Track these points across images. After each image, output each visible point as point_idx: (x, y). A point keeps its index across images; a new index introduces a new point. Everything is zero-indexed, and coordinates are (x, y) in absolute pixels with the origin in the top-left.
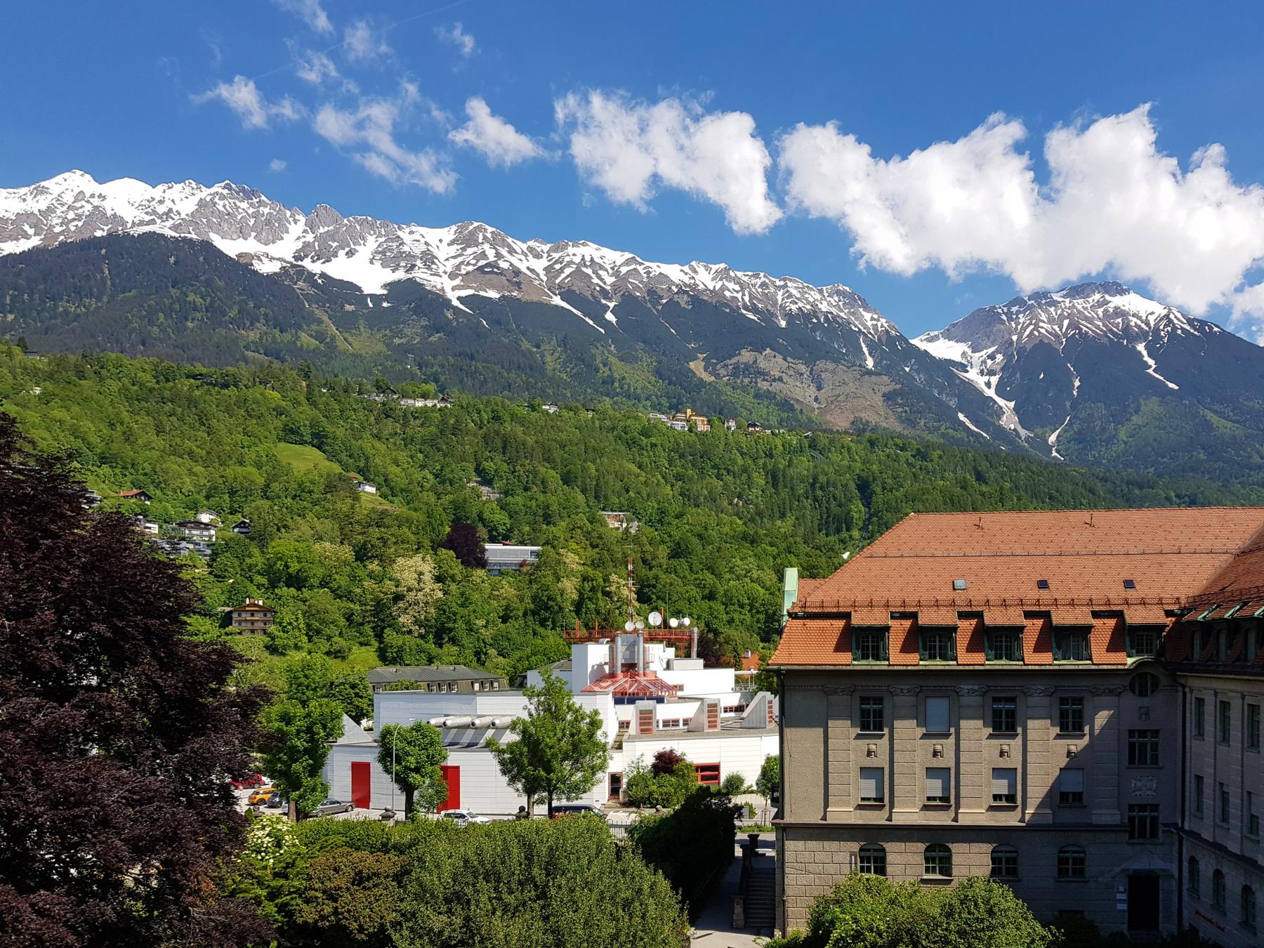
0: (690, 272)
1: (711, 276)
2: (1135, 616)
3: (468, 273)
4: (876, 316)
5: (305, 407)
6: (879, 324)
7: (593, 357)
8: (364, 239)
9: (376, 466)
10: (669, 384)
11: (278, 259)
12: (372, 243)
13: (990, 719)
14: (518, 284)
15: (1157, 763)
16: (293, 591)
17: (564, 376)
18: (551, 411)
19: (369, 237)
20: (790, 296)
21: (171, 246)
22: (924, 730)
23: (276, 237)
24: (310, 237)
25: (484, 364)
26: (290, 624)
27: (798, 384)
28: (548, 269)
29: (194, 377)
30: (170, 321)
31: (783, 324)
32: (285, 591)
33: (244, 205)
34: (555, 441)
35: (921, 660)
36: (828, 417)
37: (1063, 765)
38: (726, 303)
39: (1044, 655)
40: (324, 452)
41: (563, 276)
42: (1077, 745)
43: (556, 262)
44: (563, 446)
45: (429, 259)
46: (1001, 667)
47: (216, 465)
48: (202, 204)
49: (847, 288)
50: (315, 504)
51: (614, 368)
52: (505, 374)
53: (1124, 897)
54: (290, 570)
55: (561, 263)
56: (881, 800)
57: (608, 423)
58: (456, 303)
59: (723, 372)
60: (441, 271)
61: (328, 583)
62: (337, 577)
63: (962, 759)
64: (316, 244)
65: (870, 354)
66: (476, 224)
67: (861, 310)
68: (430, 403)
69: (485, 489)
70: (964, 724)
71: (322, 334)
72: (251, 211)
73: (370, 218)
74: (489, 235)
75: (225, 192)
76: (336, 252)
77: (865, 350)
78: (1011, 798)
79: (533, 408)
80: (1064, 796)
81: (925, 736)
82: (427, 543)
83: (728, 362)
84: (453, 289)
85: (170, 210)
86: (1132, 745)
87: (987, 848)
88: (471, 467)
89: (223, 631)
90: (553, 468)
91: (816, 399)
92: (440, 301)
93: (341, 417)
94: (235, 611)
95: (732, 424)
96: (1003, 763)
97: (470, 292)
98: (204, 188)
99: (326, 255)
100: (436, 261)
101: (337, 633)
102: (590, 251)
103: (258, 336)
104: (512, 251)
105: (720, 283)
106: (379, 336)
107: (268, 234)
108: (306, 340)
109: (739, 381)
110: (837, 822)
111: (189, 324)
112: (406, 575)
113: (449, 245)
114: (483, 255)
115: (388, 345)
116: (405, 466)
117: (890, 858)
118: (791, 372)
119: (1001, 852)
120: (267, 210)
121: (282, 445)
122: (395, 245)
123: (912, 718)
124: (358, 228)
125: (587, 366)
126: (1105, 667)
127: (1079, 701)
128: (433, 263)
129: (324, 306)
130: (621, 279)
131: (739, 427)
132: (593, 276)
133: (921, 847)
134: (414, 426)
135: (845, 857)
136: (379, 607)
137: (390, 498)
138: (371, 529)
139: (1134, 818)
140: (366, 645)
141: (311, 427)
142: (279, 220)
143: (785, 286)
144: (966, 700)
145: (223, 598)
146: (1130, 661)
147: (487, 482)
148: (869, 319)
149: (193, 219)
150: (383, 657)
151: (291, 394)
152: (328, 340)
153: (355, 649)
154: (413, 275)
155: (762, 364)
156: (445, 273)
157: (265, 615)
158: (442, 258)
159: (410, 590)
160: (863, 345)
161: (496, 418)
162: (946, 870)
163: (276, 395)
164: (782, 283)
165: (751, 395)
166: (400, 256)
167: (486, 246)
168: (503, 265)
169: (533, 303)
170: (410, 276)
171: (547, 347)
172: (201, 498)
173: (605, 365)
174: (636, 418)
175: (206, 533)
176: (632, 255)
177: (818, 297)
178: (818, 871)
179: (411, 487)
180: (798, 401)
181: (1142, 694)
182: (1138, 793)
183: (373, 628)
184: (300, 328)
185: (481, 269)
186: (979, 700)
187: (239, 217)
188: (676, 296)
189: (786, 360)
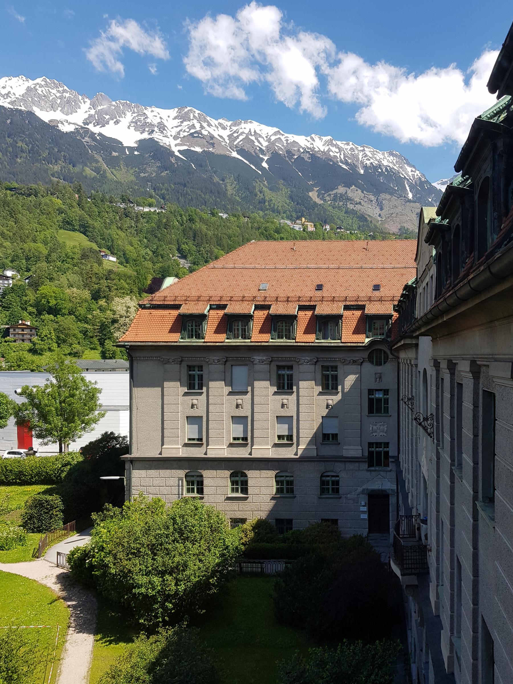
0: (311, 140)
1: (323, 143)
2: (372, 309)
3: (184, 137)
4: (414, 170)
5: (77, 209)
6: (416, 175)
7: (254, 187)
8: (125, 114)
9: (118, 245)
10: (297, 204)
11: (73, 124)
12: (129, 117)
13: (275, 380)
14: (213, 145)
15: (388, 412)
16: (52, 317)
17: (237, 198)
18: (224, 217)
19: (127, 113)
20: (366, 156)
21: (8, 113)
22: (230, 389)
23: (73, 111)
24: (93, 112)
25: (191, 190)
26: (46, 336)
27: (370, 206)
28: (230, 136)
29: (11, 189)
30: (5, 157)
31: (362, 172)
32: (47, 317)
33: (54, 91)
34: (225, 234)
35: (227, 339)
36: (386, 226)
37: (324, 414)
38: (330, 159)
39: (309, 336)
40: (87, 236)
41: (238, 140)
42: (334, 399)
43: (235, 132)
44: (230, 237)
45: (162, 127)
46: (279, 344)
47: (19, 242)
48: (29, 89)
49: (398, 153)
50: (74, 265)
51: (266, 194)
52: (203, 196)
53: (365, 509)
54: (50, 305)
55: (237, 133)
56: (200, 439)
57: (256, 225)
58: (177, 154)
59: (328, 198)
60: (169, 135)
61: (74, 313)
62: (79, 308)
63: (256, 410)
64: (96, 115)
65: (410, 191)
66: (189, 108)
67: (406, 165)
68: (152, 210)
69: (182, 261)
70: (257, 384)
71: (98, 169)
72: (58, 95)
73: (128, 102)
74: (197, 115)
75: (43, 83)
76: (108, 122)
77: (408, 188)
78: (290, 437)
79: (213, 214)
80: (326, 437)
81: (230, 393)
82: (136, 289)
83: (331, 193)
84: (176, 145)
85: (9, 92)
86: (371, 401)
87: (272, 473)
88: (174, 247)
89: (3, 340)
90: (223, 250)
91: (380, 215)
92: (167, 152)
93: (99, 216)
94: (11, 328)
95: (328, 227)
96: (284, 413)
97: (186, 148)
98: (30, 81)
99: (103, 123)
100: (166, 128)
101: (76, 342)
102: (254, 126)
103: (60, 168)
104: (209, 125)
105: (328, 147)
106: (132, 171)
107: (68, 109)
108: (88, 171)
109: (337, 204)
110: (143, 456)
111: (19, 160)
112: (119, 308)
113: (173, 119)
114: (193, 126)
115: (137, 177)
116: (136, 246)
117: (206, 482)
118: (366, 200)
119: (283, 476)
120: (67, 95)
121: (62, 231)
122: (142, 118)
123: (221, 380)
124: (122, 107)
125: (250, 193)
126: (349, 344)
127: (335, 368)
128: (164, 129)
129: (100, 152)
130: (272, 144)
131: (331, 229)
132: (256, 141)
133: (227, 473)
134: (144, 224)
135: (174, 481)
136: (103, 327)
137: (125, 264)
138: (102, 281)
139: (373, 452)
140: (94, 349)
141: (80, 221)
142: (75, 101)
143: (364, 150)
144: (259, 367)
145: (5, 320)
146: (367, 340)
147: (184, 257)
148: (410, 171)
149: (23, 98)
150: (104, 356)
151: (68, 201)
152: (102, 172)
153: (86, 352)
154: (153, 136)
155: (350, 194)
156: (171, 136)
157: (31, 331)
158: (169, 128)
159: (121, 317)
160: (407, 186)
161: (191, 220)
162: (245, 490)
163: (59, 201)
164: (362, 149)
165: (343, 212)
166: (145, 124)
167: (195, 122)
168: (205, 133)
169: (221, 155)
170: (151, 137)
171: (228, 181)
172: (7, 261)
173: (261, 192)
174: (272, 222)
175: (6, 282)
176: (277, 130)
177: (382, 157)
178: (155, 492)
179: (138, 258)
180: (369, 216)
181: (379, 364)
182: (375, 434)
183: (98, 339)
184: (86, 165)
185: (192, 134)
186: (267, 367)
187: (51, 98)
188: (302, 154)
189: (363, 193)
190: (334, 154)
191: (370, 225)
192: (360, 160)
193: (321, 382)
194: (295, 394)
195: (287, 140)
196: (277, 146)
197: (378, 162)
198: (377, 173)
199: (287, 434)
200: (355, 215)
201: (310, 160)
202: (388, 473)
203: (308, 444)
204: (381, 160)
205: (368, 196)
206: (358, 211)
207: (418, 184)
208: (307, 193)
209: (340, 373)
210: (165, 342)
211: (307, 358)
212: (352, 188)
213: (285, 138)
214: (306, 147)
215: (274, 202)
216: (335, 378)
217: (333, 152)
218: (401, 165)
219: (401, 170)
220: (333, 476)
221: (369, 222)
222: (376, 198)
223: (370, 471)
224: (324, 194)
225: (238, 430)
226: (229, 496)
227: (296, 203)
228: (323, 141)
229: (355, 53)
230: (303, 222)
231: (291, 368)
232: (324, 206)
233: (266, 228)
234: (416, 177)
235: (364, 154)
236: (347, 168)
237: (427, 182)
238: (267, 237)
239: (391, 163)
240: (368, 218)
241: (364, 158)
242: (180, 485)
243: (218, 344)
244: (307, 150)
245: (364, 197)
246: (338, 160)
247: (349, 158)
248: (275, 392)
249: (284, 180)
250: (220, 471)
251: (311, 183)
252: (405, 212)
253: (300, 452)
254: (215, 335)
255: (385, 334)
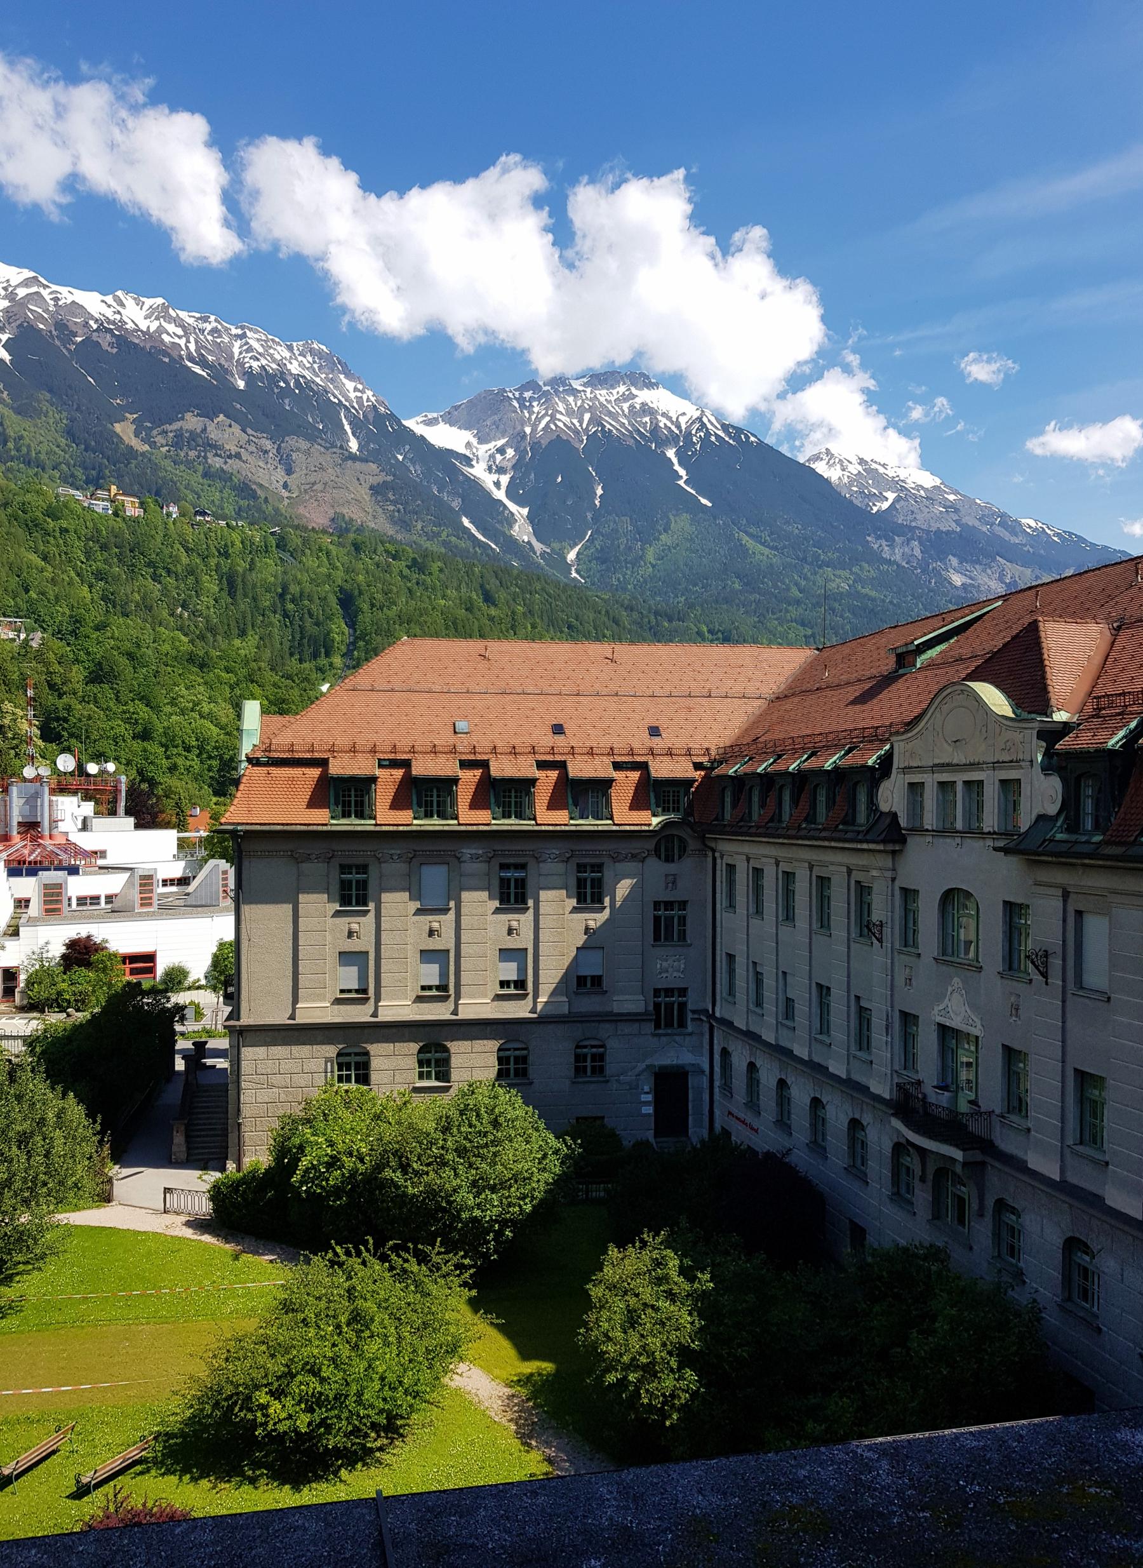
0: (114, 304)
1: (144, 313)
4: (360, 387)
15: (684, 939)
20: (250, 349)
22: (418, 905)
27: (261, 464)
31: (241, 384)
37: (580, 944)
42: (596, 919)
46: (509, 828)
53: (649, 1098)
56: (364, 991)
59: (160, 440)
63: (463, 939)
65: (354, 434)
67: (342, 376)
70: (465, 896)
77: (347, 428)
78: (520, 984)
80: (581, 981)
81: (419, 912)
87: (493, 1045)
91: (285, 486)
95: (174, 510)
105: (157, 323)
118: (252, 448)
119: (509, 1050)
123: (403, 890)
127: (598, 868)
135: (317, 1065)
143: (244, 336)
144: (469, 867)
146: (655, 821)
148: (351, 390)
155: (213, 434)
164: (239, 332)
165: (199, 474)
176: (32, 274)
177: (287, 354)
178: (284, 1084)
180: (261, 486)
181: (669, 859)
182: (664, 975)
189: (245, 432)
190: (172, 340)
191: (264, 506)
192: (236, 358)
193: (575, 890)
194: (531, 911)
195: (56, 299)
196: (31, 311)
197: (279, 365)
198: (276, 391)
199: (515, 978)
200: (228, 484)
201: (115, 350)
202: (688, 1038)
203: (552, 994)
204: (284, 361)
205: (257, 441)
206: (235, 473)
207: (371, 421)
208: (109, 425)
209: (608, 874)
210: (305, 825)
211: (554, 851)
212: (218, 419)
213: (51, 293)
214: (103, 318)
215: (27, 441)
216: (598, 884)
217: (168, 334)
218: (331, 376)
219: (331, 386)
220: (593, 1047)
221: (261, 500)
222: (276, 447)
223: (659, 1035)
224: (151, 429)
225: (431, 974)
226: (417, 1085)
227: (83, 446)
228: (146, 307)
229: (272, 134)
230: (112, 494)
231: (522, 867)
232: (153, 458)
233: (24, 504)
234: (366, 404)
235: (245, 344)
236: (204, 374)
237: (392, 417)
238: (27, 525)
239: (308, 368)
240: (259, 492)
241: (244, 354)
242: (329, 1070)
243: (401, 828)
244: (106, 325)
245: (249, 441)
246: (182, 353)
247: (210, 352)
248: (497, 908)
249: (50, 391)
250: (401, 1044)
251: (118, 401)
252: (343, 482)
253: (539, 1007)
254: (393, 812)
255: (682, 809)
